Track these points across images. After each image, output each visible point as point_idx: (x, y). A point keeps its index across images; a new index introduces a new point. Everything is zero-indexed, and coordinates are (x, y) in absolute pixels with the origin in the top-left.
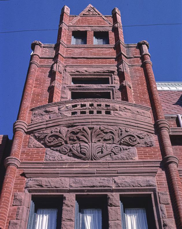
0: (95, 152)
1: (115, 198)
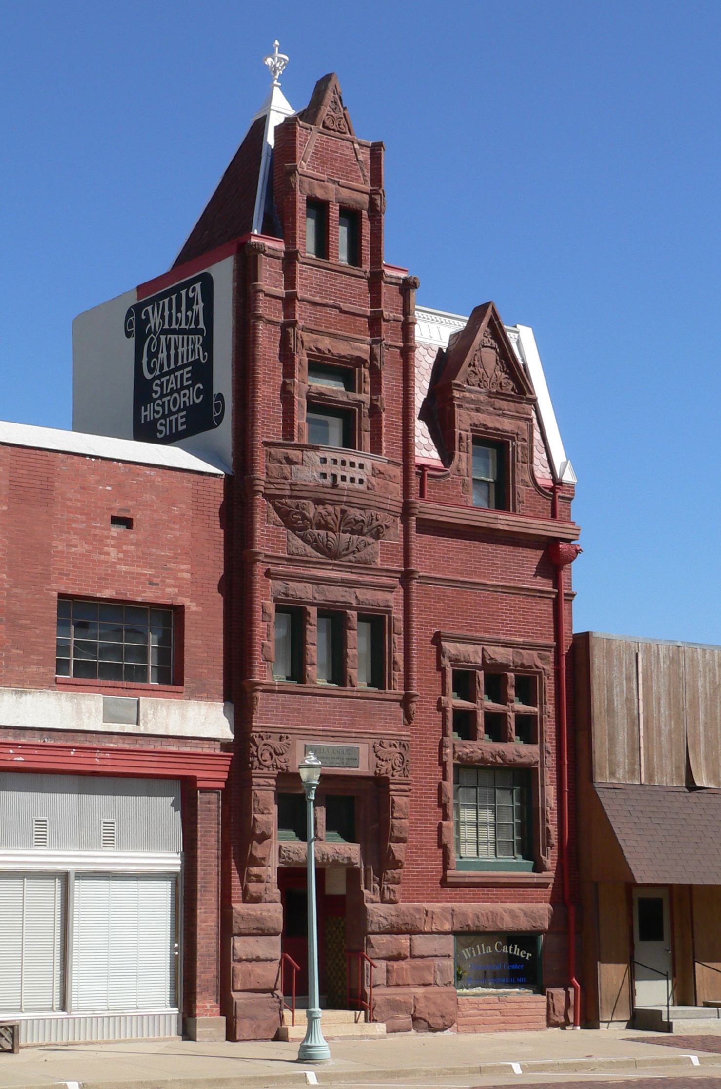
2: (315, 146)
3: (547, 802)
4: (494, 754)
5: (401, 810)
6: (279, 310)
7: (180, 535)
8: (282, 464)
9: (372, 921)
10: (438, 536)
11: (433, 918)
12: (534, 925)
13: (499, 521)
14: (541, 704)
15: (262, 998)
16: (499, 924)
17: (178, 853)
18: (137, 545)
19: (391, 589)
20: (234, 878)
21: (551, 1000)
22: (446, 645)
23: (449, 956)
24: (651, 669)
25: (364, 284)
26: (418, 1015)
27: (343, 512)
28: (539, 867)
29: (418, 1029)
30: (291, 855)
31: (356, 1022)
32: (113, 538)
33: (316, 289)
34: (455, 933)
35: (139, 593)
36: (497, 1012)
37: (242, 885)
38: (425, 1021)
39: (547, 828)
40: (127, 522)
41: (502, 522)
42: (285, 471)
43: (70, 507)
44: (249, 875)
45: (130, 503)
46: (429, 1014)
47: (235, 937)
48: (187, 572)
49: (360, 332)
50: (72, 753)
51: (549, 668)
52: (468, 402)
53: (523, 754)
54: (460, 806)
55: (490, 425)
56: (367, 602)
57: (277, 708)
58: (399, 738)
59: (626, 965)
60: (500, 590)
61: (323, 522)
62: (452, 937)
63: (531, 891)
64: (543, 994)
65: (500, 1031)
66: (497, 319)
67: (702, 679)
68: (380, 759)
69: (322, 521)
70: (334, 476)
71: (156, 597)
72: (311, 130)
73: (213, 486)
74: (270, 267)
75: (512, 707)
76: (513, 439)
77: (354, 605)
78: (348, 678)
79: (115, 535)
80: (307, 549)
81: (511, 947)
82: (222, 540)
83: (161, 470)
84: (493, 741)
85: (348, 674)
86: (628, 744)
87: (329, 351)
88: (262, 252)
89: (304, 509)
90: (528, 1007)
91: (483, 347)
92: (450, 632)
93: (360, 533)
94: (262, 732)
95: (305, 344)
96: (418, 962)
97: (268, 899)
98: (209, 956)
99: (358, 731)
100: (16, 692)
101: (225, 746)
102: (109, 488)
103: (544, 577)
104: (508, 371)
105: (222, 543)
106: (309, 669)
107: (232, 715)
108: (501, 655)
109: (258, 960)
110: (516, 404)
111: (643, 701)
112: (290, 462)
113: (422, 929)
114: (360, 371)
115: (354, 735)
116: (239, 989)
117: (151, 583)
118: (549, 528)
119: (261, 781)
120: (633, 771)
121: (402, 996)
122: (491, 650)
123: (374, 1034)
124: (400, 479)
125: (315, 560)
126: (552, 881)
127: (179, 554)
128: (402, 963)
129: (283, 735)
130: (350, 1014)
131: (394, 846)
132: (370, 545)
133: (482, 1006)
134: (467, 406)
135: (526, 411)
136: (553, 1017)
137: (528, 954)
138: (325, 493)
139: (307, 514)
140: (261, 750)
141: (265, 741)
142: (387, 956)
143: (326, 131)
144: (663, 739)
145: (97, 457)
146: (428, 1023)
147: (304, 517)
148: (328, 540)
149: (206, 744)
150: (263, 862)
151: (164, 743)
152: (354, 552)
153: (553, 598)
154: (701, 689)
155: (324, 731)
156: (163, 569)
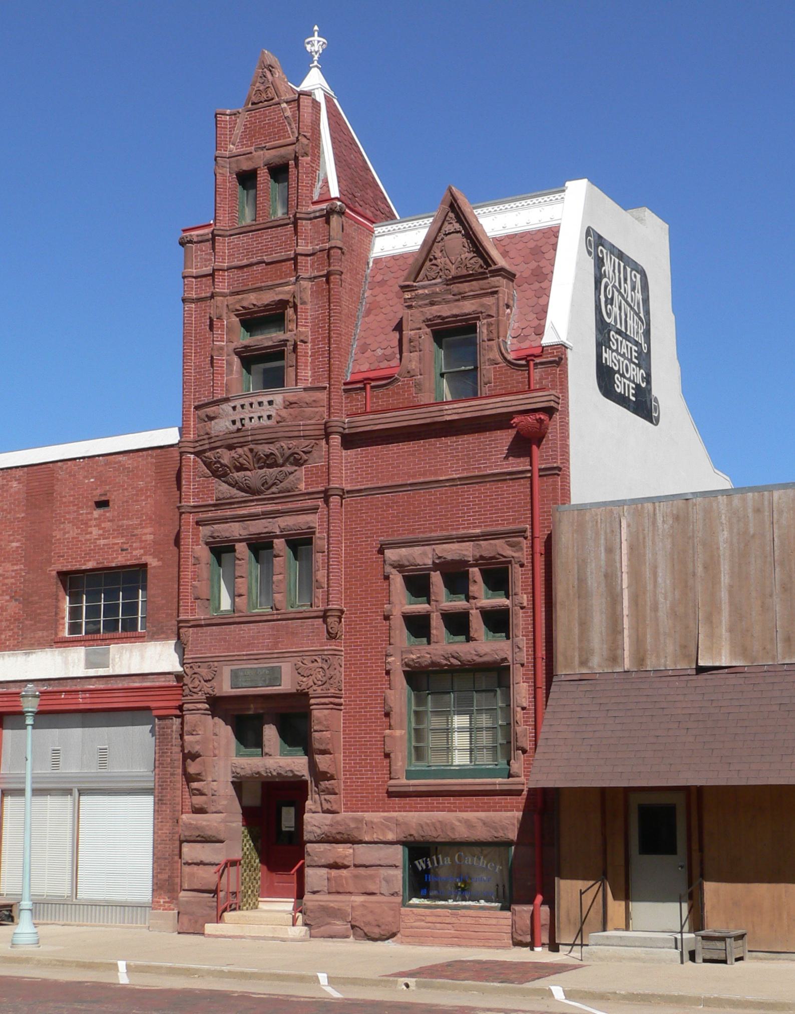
4: (446, 656)
5: (320, 723)
13: (445, 412)
16: (449, 833)
19: (314, 510)
23: (397, 867)
26: (354, 923)
27: (251, 450)
29: (357, 937)
32: (95, 519)
40: (102, 504)
41: (449, 412)
43: (65, 503)
45: (108, 488)
49: (286, 276)
50: (63, 696)
51: (523, 555)
52: (422, 299)
53: (482, 652)
55: (445, 314)
57: (205, 640)
60: (459, 483)
61: (238, 464)
62: (400, 848)
65: (452, 945)
66: (456, 201)
67: (726, 533)
68: (302, 676)
71: (126, 560)
72: (239, 113)
77: (278, 533)
87: (254, 305)
91: (446, 235)
92: (400, 538)
95: (230, 307)
96: (362, 871)
100: (26, 654)
102: (92, 480)
103: (519, 456)
108: (452, 551)
109: (202, 863)
115: (275, 656)
116: (186, 888)
118: (509, 404)
120: (614, 658)
125: (240, 499)
127: (144, 520)
128: (344, 872)
132: (292, 473)
133: (429, 919)
134: (420, 303)
135: (493, 284)
137: (498, 867)
142: (325, 863)
143: (255, 106)
145: (83, 458)
147: (222, 465)
149: (162, 678)
150: (199, 777)
152: (274, 484)
154: (723, 546)
155: (246, 655)
156: (131, 536)
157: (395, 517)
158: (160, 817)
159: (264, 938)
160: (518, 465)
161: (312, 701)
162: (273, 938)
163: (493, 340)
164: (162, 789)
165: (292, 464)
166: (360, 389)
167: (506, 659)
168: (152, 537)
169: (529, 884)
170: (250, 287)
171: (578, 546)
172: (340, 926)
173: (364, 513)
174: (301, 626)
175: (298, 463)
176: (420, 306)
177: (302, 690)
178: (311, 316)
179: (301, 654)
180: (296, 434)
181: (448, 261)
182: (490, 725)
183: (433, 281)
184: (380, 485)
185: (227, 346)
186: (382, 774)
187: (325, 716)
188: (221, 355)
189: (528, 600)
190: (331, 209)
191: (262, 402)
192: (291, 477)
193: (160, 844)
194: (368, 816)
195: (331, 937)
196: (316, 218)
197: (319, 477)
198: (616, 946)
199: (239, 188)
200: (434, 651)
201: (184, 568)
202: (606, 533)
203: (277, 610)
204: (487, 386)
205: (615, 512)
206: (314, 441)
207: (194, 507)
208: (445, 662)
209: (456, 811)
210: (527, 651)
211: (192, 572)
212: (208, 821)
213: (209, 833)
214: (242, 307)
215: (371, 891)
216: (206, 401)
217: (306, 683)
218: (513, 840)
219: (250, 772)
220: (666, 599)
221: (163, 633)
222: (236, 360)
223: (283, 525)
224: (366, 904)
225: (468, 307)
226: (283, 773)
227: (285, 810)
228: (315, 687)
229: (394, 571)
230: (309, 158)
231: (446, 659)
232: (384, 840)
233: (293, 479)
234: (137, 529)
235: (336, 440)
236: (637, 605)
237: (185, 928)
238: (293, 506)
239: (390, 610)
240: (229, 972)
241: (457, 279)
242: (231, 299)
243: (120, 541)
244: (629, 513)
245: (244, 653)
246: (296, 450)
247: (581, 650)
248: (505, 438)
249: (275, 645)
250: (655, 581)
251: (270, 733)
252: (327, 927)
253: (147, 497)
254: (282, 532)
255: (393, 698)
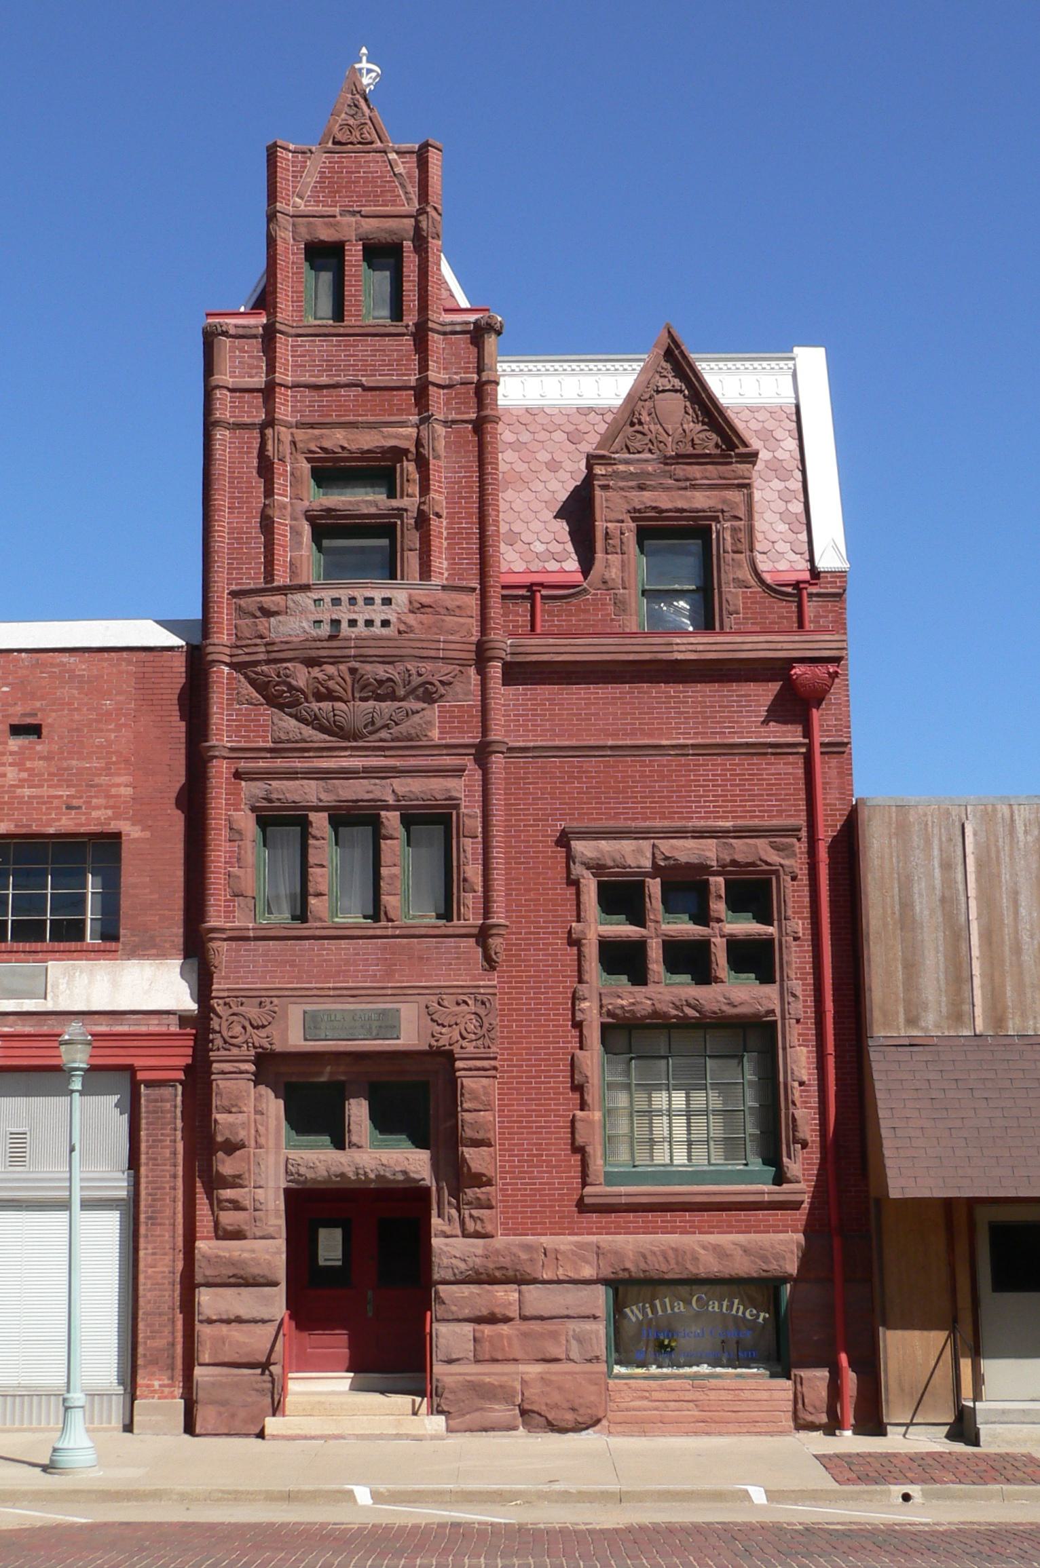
0: (360, 724)
1: (392, 820)
2: (320, 172)
3: (792, 1073)
5: (476, 1098)
6: (257, 408)
7: (116, 737)
8: (257, 618)
9: (439, 1267)
10: (568, 684)
11: (557, 1259)
12: (765, 1268)
13: (676, 648)
14: (780, 920)
15: (245, 1375)
16: (689, 1266)
17: (123, 1173)
18: (48, 758)
19: (458, 772)
20: (201, 1204)
21: (799, 1387)
22: (578, 846)
23: (595, 1317)
24: (997, 846)
25: (408, 342)
26: (527, 1407)
27: (353, 671)
28: (780, 1178)
29: (530, 1427)
30: (303, 1170)
31: (415, 1413)
32: (12, 753)
33: (322, 366)
34: (606, 1282)
35: (49, 823)
36: (691, 1404)
37: (213, 1214)
38: (540, 1415)
39: (793, 1114)
40: (35, 730)
41: (682, 648)
42: (260, 627)
44: (220, 1201)
45: (38, 704)
46: (547, 1405)
47: (202, 1289)
48: (126, 786)
49: (400, 411)
51: (797, 863)
52: (623, 479)
53: (736, 1000)
54: (633, 1088)
56: (412, 796)
57: (254, 961)
58: (473, 991)
59: (947, 1333)
60: (691, 752)
62: (601, 1289)
63: (763, 1215)
64: (789, 1378)
65: (696, 1433)
66: (678, 346)
68: (438, 1025)
69: (321, 688)
70: (336, 623)
71: (77, 825)
73: (169, 664)
74: (240, 352)
75: (721, 930)
76: (716, 519)
77: (391, 802)
78: (382, 908)
79: (16, 749)
80: (303, 731)
81: (725, 1303)
82: (184, 735)
83: (87, 654)
84: (761, 983)
85: (382, 903)
86: (946, 972)
87: (343, 448)
88: (220, 335)
89: (288, 677)
90: (752, 1398)
91: (658, 392)
93: (393, 697)
94: (229, 997)
95: (299, 445)
96: (535, 1326)
97: (258, 1234)
98: (160, 1314)
99: (399, 985)
101: (184, 1019)
102: (5, 689)
104: (706, 420)
105: (184, 740)
106: (313, 902)
107: (195, 976)
108: (685, 850)
109: (239, 1320)
110: (719, 467)
111: (976, 898)
112: (267, 613)
113: (538, 1276)
114: (402, 467)
115: (389, 992)
116: (207, 1361)
117: (69, 808)
118: (779, 646)
119: (227, 1067)
120: (958, 1015)
121: (497, 1377)
122: (665, 846)
123: (422, 1432)
124: (475, 611)
126: (807, 1199)
127: (114, 763)
128: (504, 1328)
129: (263, 999)
130: (404, 1401)
131: (468, 1153)
132: (418, 712)
133: (656, 1395)
134: (622, 484)
136: (801, 1414)
137: (762, 1315)
138: (318, 649)
139: (294, 683)
140: (223, 1024)
141: (235, 1009)
142: (471, 1316)
143: (338, 148)
144: (1025, 958)
146: (547, 1419)
147: (291, 688)
148: (335, 715)
149: (154, 1020)
151: (86, 1022)
152: (387, 726)
153: (802, 753)
155: (334, 989)
157: (584, 793)
158: (150, 1246)
159: (380, 1437)
160: (784, 734)
161: (459, 1064)
162: (398, 1436)
163: (742, 553)
164: (154, 1200)
165: (418, 699)
166: (523, 597)
167: (773, 1011)
168: (130, 791)
169: (815, 1338)
170: (334, 419)
171: (898, 857)
172: (502, 1412)
173: (530, 783)
174: (437, 948)
175: (429, 697)
176: (622, 489)
177: (438, 1047)
178: (446, 478)
179: (438, 992)
180: (433, 653)
181: (661, 430)
182: (720, 1107)
183: (637, 456)
184: (557, 743)
185: (292, 504)
186: (567, 1178)
187: (484, 1087)
188: (283, 517)
189: (803, 929)
190: (488, 324)
191: (372, 599)
192: (416, 718)
193: (150, 1290)
194: (547, 1241)
195: (486, 1430)
196: (454, 333)
197: (465, 722)
198: (1018, 1423)
199: (306, 265)
200: (659, 996)
201: (215, 845)
202: (940, 839)
203: (392, 921)
204: (732, 617)
205: (954, 813)
206: (458, 668)
207: (232, 749)
208: (674, 1012)
209: (695, 1233)
210: (805, 1001)
211: (226, 852)
212: (253, 1251)
213: (256, 1271)
214: (321, 448)
215: (553, 1357)
216: (252, 586)
217: (446, 1037)
218: (792, 1275)
219: (325, 1174)
220: (1032, 937)
221: (154, 946)
222: (306, 529)
223: (401, 790)
224: (548, 1376)
225: (701, 500)
226: (388, 1174)
227: (323, 1233)
228: (465, 1043)
229: (587, 874)
230: (440, 243)
231: (677, 1007)
232: (576, 1277)
233: (421, 722)
234: (100, 775)
235: (495, 670)
236: (990, 943)
237: (210, 1427)
238: (306, 765)
239: (583, 932)
240: (580, 1492)
241: (680, 458)
242: (300, 434)
243: (64, 792)
244: (974, 816)
245: (331, 985)
246: (430, 679)
247: (908, 1004)
248: (766, 693)
249: (389, 974)
250: (1016, 913)
251: (358, 1111)
252: (477, 1414)
253: (119, 727)
254: (399, 801)
255: (589, 1062)
